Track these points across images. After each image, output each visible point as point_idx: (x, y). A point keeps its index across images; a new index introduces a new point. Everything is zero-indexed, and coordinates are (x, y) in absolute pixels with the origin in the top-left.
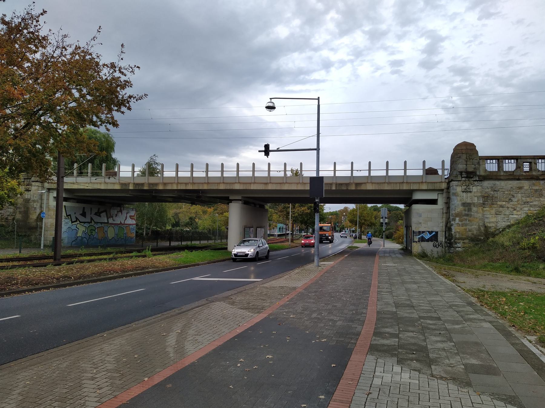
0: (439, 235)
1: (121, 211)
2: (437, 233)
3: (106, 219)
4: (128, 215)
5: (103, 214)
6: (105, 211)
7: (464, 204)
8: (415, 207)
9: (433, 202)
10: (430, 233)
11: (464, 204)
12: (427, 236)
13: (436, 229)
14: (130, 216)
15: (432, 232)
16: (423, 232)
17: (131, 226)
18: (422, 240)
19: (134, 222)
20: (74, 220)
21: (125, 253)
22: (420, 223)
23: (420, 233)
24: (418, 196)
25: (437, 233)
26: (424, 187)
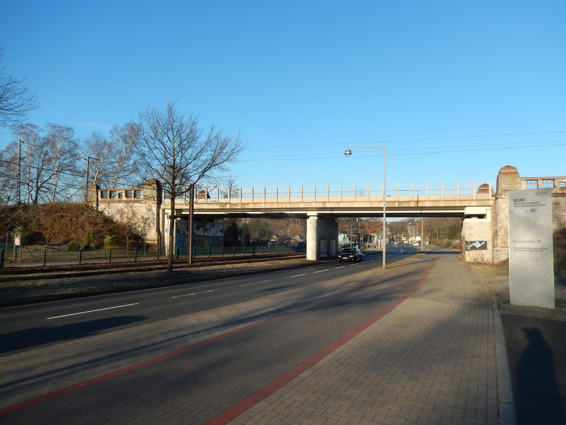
0: (488, 245)
1: (213, 226)
2: (486, 242)
3: (203, 232)
4: (218, 229)
5: (201, 229)
6: (202, 226)
7: (47, 151)
8: (466, 220)
9: (481, 216)
10: (481, 242)
11: (47, 151)
12: (478, 245)
13: (485, 240)
14: (220, 230)
15: (482, 242)
16: (474, 242)
17: (220, 239)
18: (474, 248)
19: (223, 235)
20: (182, 233)
21: (10, 274)
22: (472, 234)
23: (472, 242)
24: (467, 211)
25: (486, 242)
26: (474, 203)
